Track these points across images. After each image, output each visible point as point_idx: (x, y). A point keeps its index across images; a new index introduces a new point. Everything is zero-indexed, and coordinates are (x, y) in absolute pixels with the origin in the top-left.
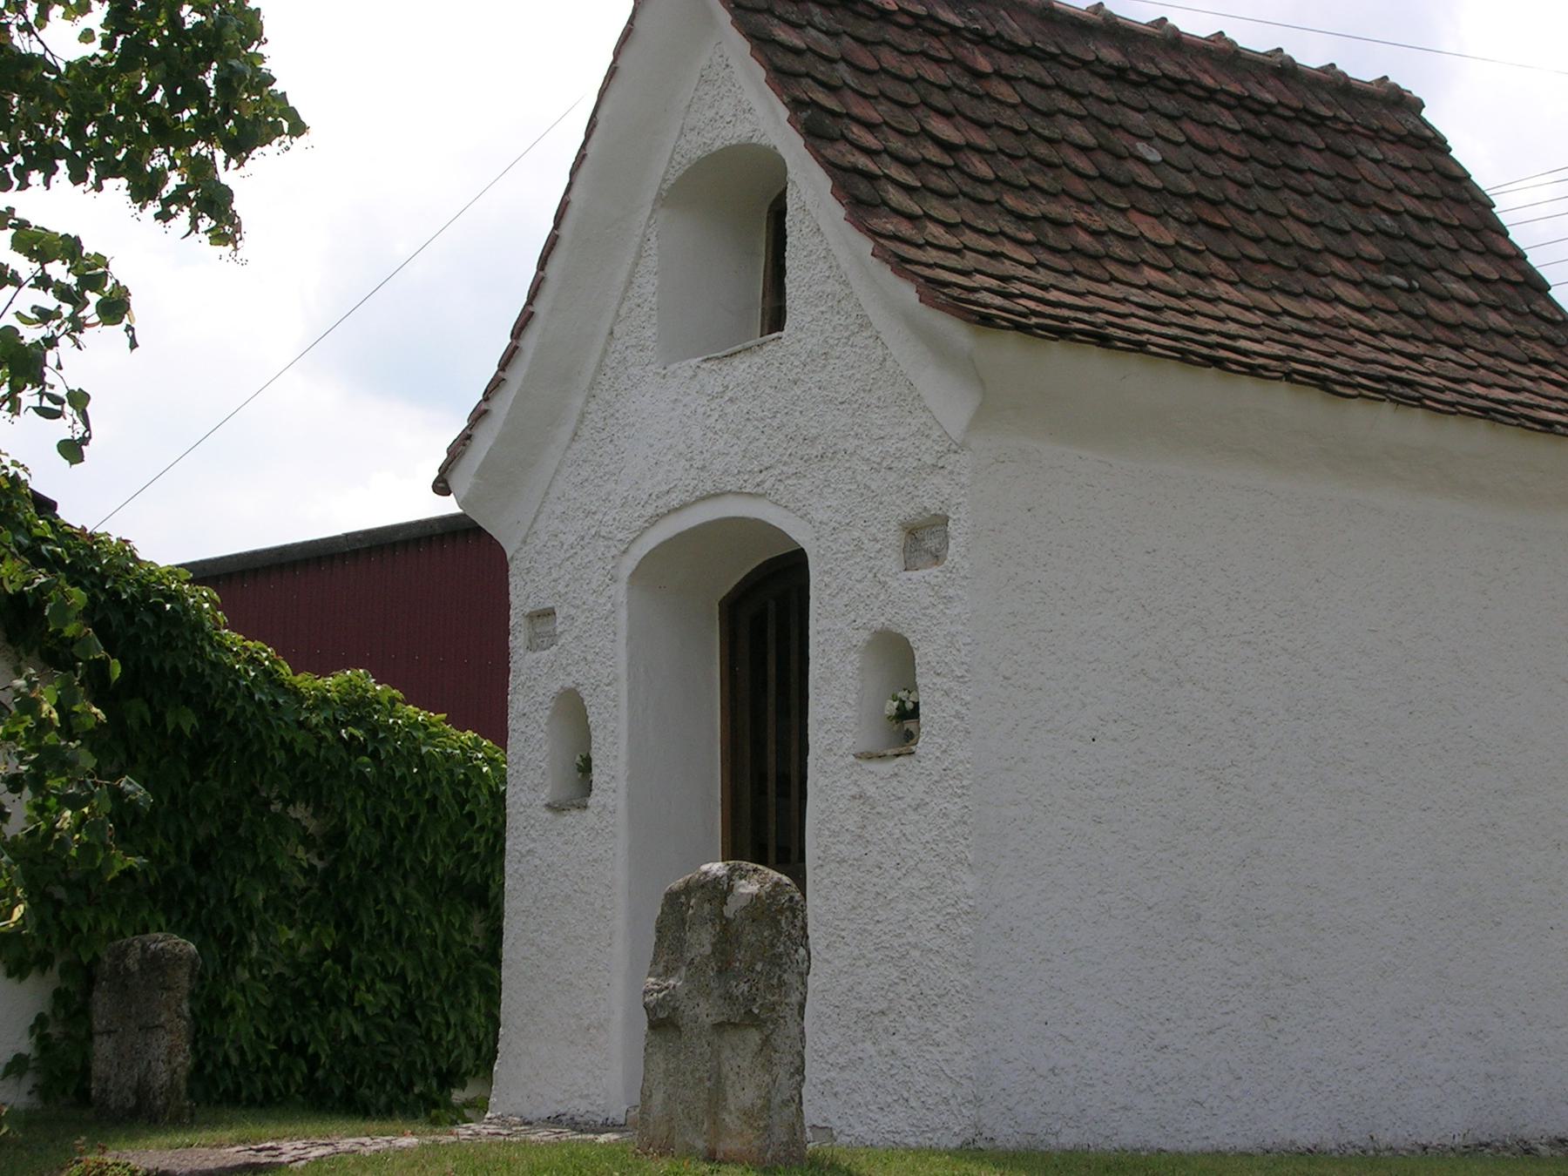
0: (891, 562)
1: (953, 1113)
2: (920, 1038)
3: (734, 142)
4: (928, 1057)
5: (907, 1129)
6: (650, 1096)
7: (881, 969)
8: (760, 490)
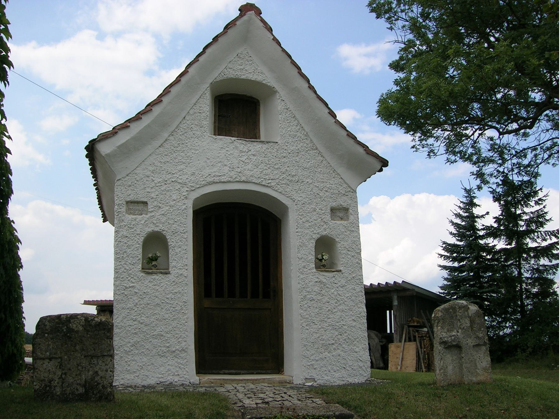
0: (328, 217)
1: (364, 371)
2: (349, 351)
3: (250, 79)
4: (352, 356)
5: (347, 376)
6: (447, 367)
7: (331, 331)
8: (269, 185)
